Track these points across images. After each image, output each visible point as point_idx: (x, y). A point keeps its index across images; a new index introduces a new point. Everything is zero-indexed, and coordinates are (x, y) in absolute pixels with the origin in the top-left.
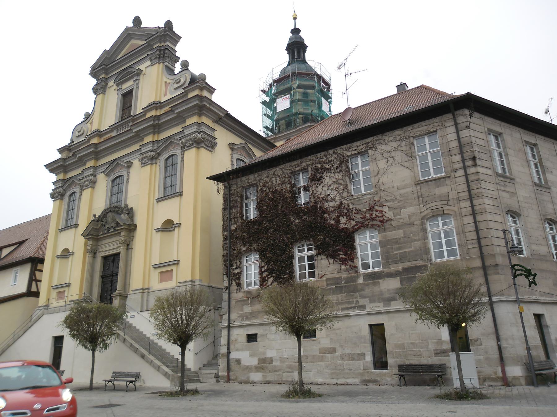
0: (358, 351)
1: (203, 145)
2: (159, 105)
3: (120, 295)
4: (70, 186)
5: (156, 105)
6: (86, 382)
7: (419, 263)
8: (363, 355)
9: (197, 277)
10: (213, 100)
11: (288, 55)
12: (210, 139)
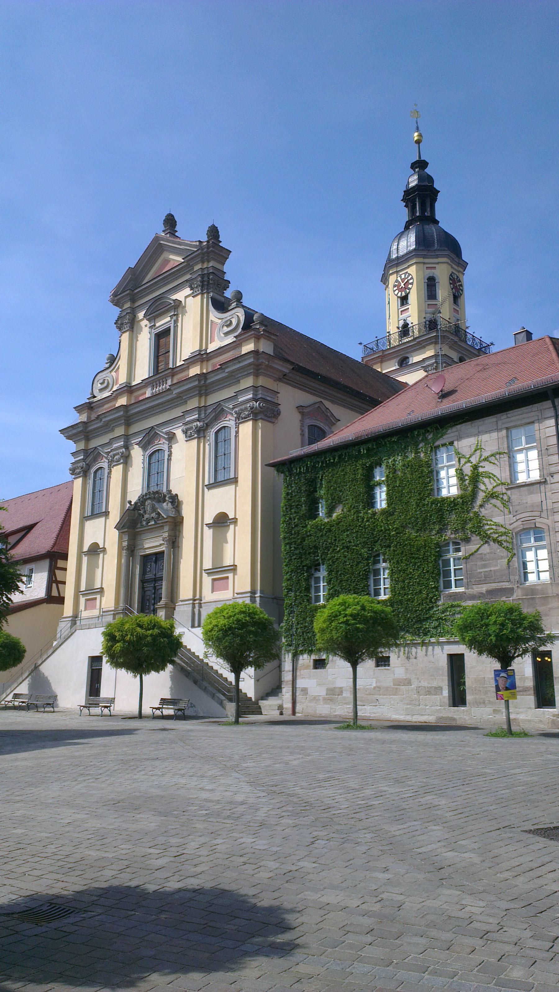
0: (435, 684)
6: (134, 709)
7: (506, 585)
8: (441, 688)
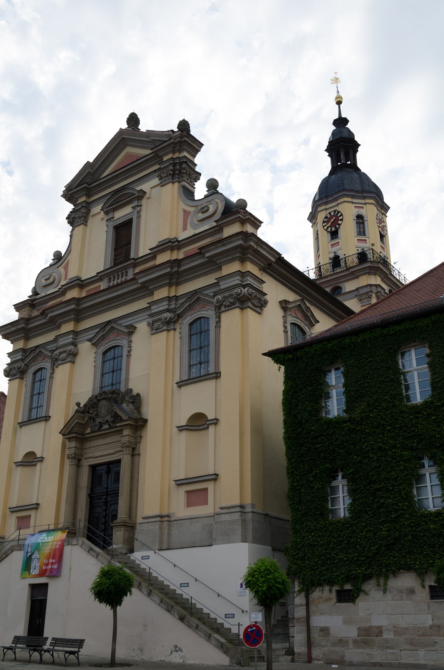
1: (250, 304)
2: (176, 243)
3: (125, 525)
4: (34, 359)
5: (171, 244)
6: (106, 654)
9: (248, 500)
10: (259, 236)
11: (329, 159)
12: (259, 296)
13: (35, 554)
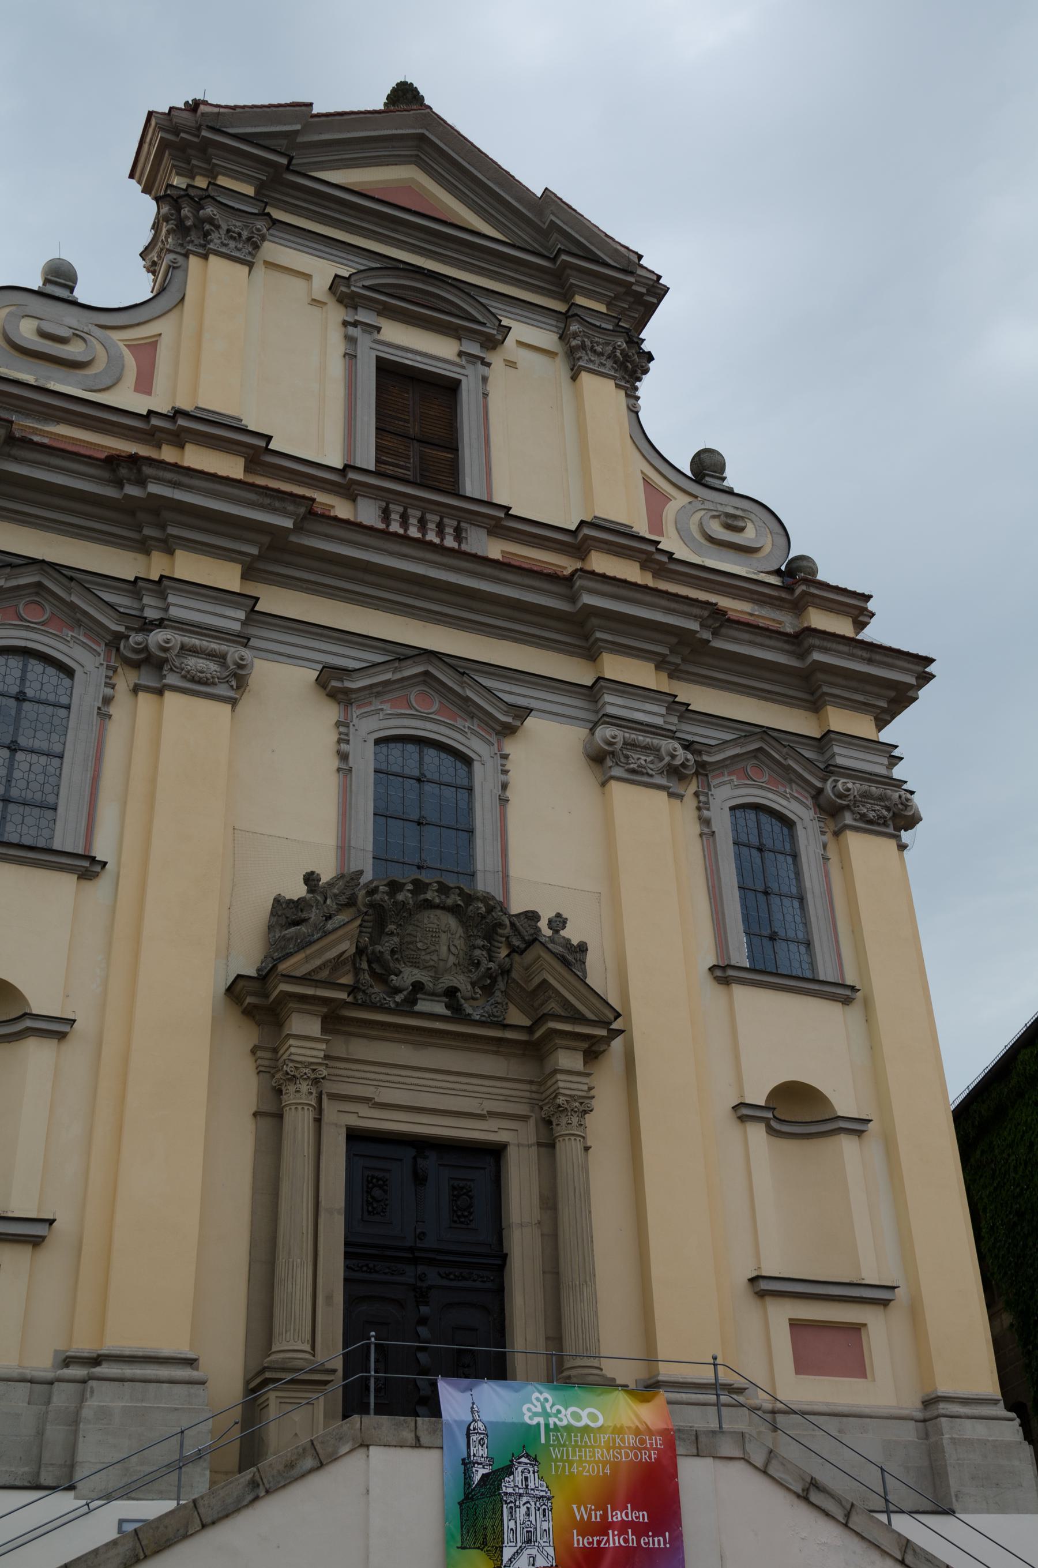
2: (665, 559)
13: (518, 1477)
